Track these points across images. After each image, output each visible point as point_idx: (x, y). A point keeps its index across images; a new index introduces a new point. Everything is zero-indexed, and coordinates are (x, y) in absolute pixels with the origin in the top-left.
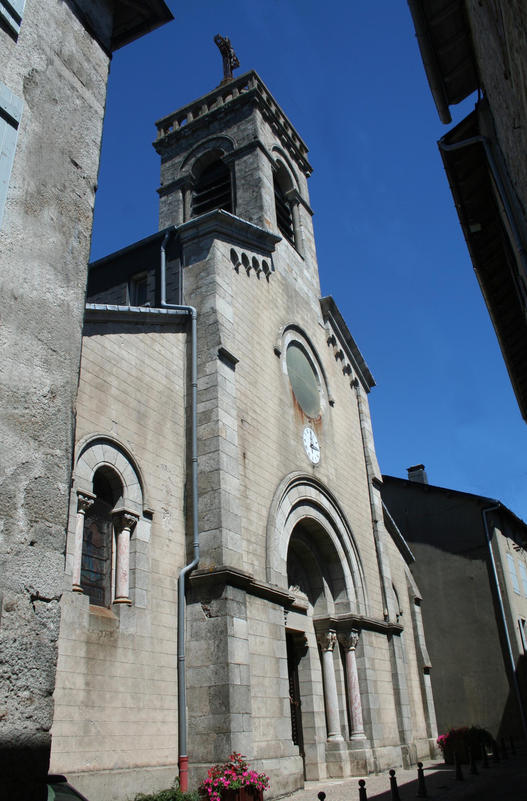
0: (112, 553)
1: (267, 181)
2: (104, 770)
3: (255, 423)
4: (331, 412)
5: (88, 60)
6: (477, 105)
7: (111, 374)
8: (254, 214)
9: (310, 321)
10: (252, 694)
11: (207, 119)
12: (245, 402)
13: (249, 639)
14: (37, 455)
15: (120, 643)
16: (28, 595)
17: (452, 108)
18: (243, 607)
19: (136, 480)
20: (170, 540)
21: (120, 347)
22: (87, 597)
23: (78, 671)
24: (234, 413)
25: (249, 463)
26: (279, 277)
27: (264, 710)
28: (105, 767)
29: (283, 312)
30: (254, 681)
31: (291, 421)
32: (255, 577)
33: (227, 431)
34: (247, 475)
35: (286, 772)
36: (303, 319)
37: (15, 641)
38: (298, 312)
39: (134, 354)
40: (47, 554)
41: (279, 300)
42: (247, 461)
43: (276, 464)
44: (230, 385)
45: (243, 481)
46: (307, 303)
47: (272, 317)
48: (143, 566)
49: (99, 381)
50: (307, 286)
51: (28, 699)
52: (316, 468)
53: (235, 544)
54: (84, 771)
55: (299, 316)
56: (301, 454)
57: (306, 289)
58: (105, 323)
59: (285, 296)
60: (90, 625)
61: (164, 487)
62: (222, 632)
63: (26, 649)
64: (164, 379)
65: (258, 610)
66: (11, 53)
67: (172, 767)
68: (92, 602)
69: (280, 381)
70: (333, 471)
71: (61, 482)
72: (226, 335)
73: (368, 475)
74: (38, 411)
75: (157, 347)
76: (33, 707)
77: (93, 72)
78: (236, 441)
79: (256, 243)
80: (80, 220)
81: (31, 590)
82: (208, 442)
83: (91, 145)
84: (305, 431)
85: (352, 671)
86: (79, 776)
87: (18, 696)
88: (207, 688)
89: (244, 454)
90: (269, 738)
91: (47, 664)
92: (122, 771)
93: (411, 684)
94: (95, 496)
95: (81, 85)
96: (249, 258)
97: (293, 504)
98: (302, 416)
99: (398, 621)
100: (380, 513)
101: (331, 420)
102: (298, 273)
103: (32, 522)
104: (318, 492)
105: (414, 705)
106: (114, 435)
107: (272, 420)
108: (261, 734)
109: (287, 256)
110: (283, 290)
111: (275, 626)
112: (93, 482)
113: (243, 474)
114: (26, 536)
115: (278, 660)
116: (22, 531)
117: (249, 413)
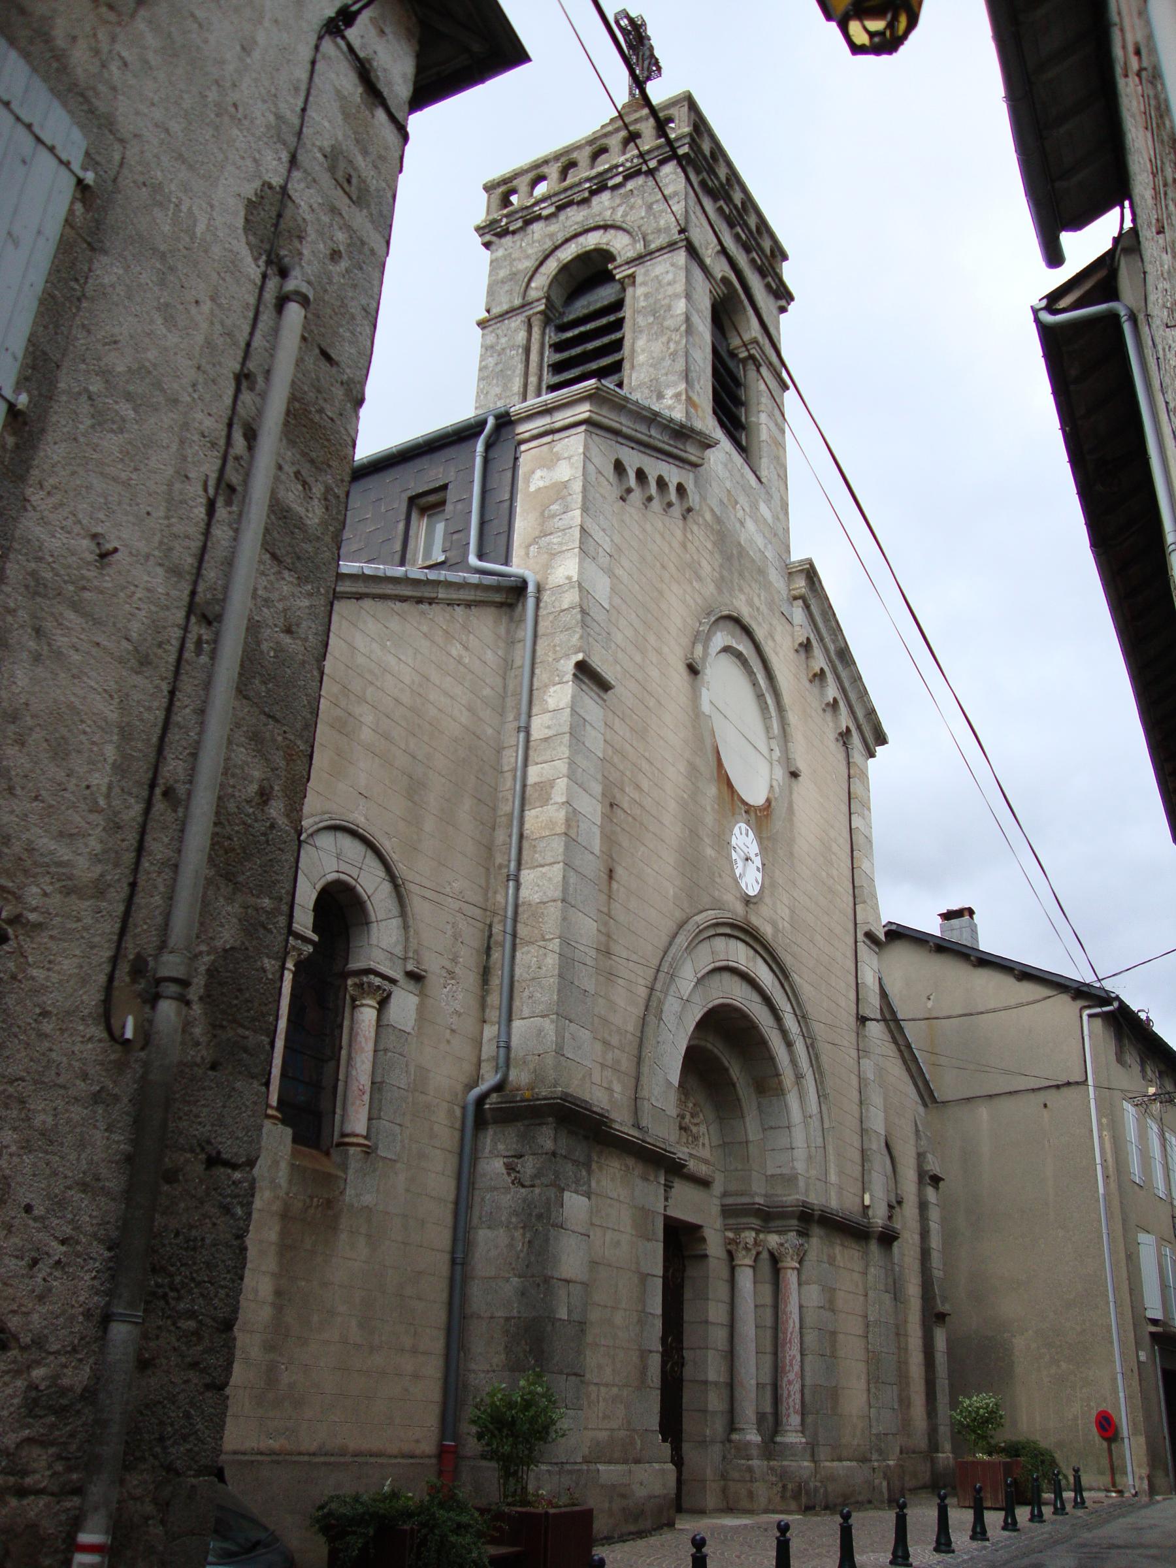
0: (341, 1048)
1: (699, 321)
2: (300, 1454)
3: (637, 811)
4: (791, 793)
5: (365, 152)
6: (1116, 241)
7: (362, 699)
8: (668, 386)
9: (763, 608)
10: (589, 1339)
11: (587, 185)
12: (621, 767)
13: (591, 1234)
14: (229, 908)
15: (344, 1223)
16: (203, 1156)
17: (1067, 239)
18: (584, 1173)
19: (395, 911)
20: (453, 1031)
21: (383, 647)
22: (289, 1131)
23: (264, 1268)
24: (597, 789)
25: (618, 890)
26: (708, 516)
27: (608, 1370)
28: (302, 1449)
29: (711, 588)
30: (594, 1315)
31: (709, 809)
32: (613, 1116)
33: (581, 824)
34: (613, 912)
35: (640, 1492)
36: (750, 603)
37: (177, 1235)
38: (741, 590)
39: (410, 661)
40: (238, 1085)
41: (704, 563)
42: (615, 885)
43: (671, 892)
44: (594, 733)
45: (606, 924)
46: (762, 572)
47: (688, 597)
48: (398, 1079)
49: (339, 712)
50: (764, 536)
51: (193, 1334)
52: (751, 906)
53: (579, 1048)
54: (262, 1453)
55: (743, 597)
56: (724, 875)
57: (760, 541)
58: (357, 599)
59: (717, 556)
60: (290, 1182)
61: (449, 927)
62: (540, 1217)
63: (194, 1249)
64: (466, 713)
65: (612, 1180)
66: (227, 158)
67: (426, 1461)
68: (296, 1140)
69: (694, 727)
70: (786, 913)
71: (268, 957)
72: (592, 633)
73: (856, 924)
74: (237, 828)
75: (456, 650)
76: (200, 1348)
77: (372, 173)
78: (597, 845)
79: (667, 447)
80: (329, 466)
81: (208, 1148)
82: (543, 844)
83: (359, 317)
84: (736, 830)
85: (788, 1309)
86: (252, 1462)
87: (178, 1328)
88: (502, 1321)
89: (611, 871)
90: (614, 1425)
91: (228, 1276)
92: (332, 1459)
93: (907, 1344)
94: (316, 938)
95: (347, 201)
96: (650, 478)
97: (699, 975)
98: (733, 800)
99: (890, 1218)
100: (873, 1002)
101: (791, 810)
102: (747, 510)
103: (215, 1026)
104: (751, 952)
105: (908, 1384)
106: (361, 820)
107: (672, 806)
108: (601, 1415)
109: (727, 474)
110: (714, 544)
111: (643, 1214)
112: (314, 910)
113: (605, 910)
114: (204, 1053)
115: (644, 1278)
116: (198, 1044)
117: (627, 790)
